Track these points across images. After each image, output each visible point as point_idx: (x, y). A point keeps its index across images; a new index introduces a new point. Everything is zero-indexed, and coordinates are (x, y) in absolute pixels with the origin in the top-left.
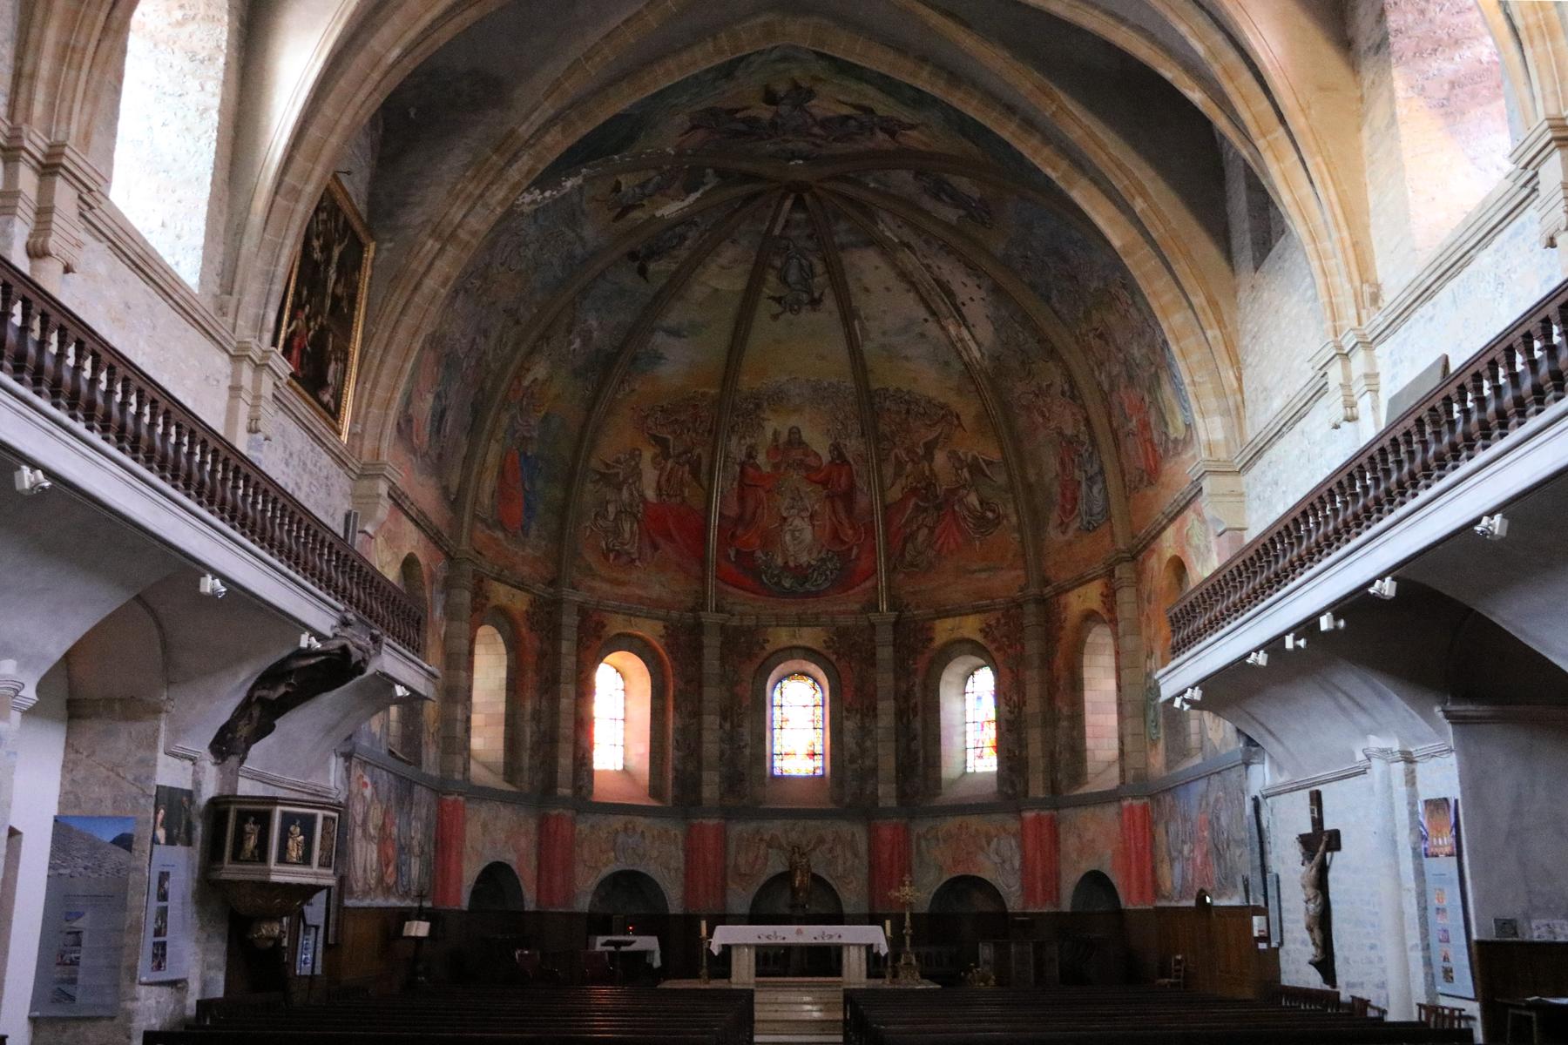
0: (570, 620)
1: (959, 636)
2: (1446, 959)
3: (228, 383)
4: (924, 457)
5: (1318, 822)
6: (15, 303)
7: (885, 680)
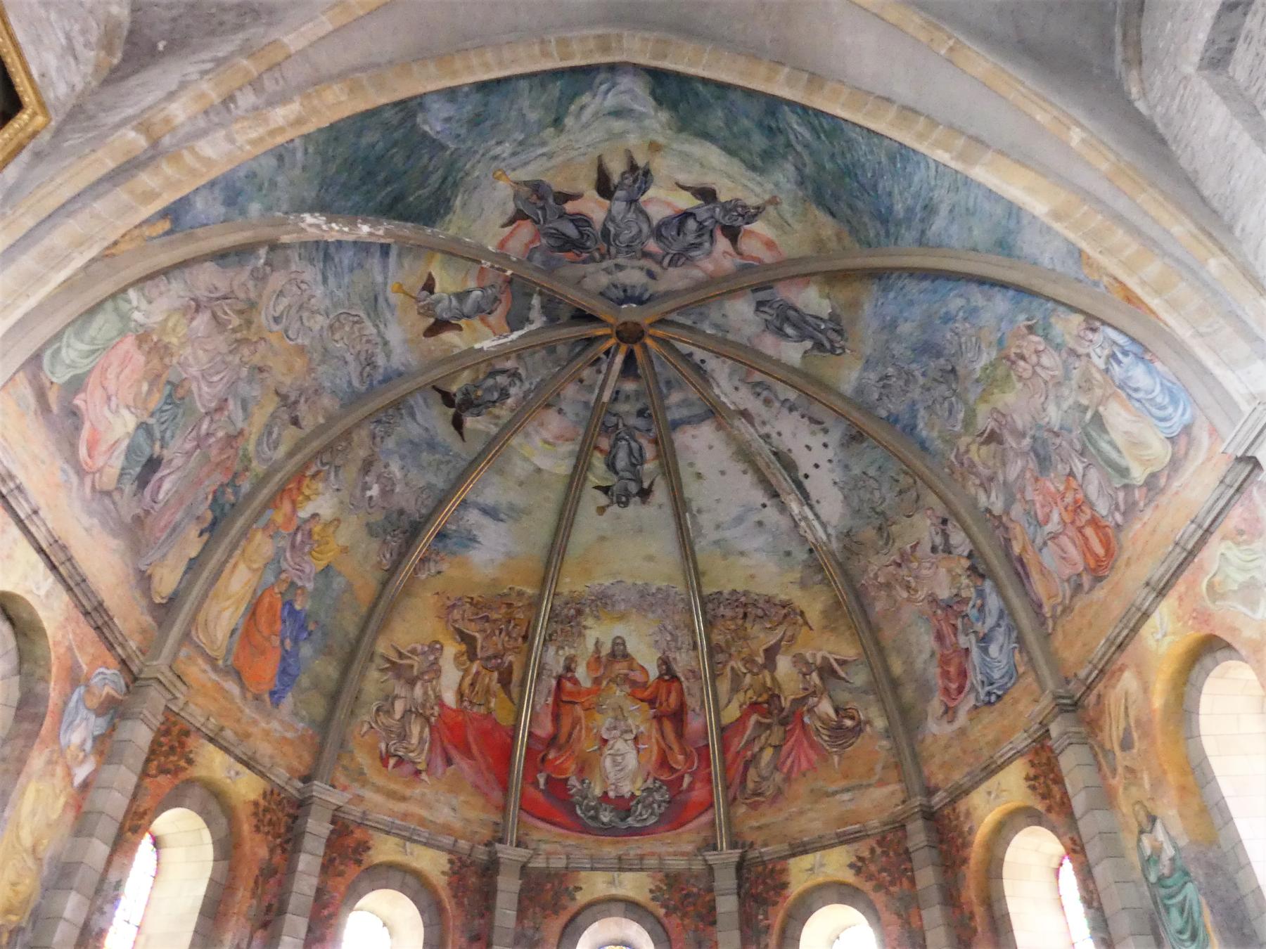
0: (317, 828)
1: (821, 879)
4: (764, 666)
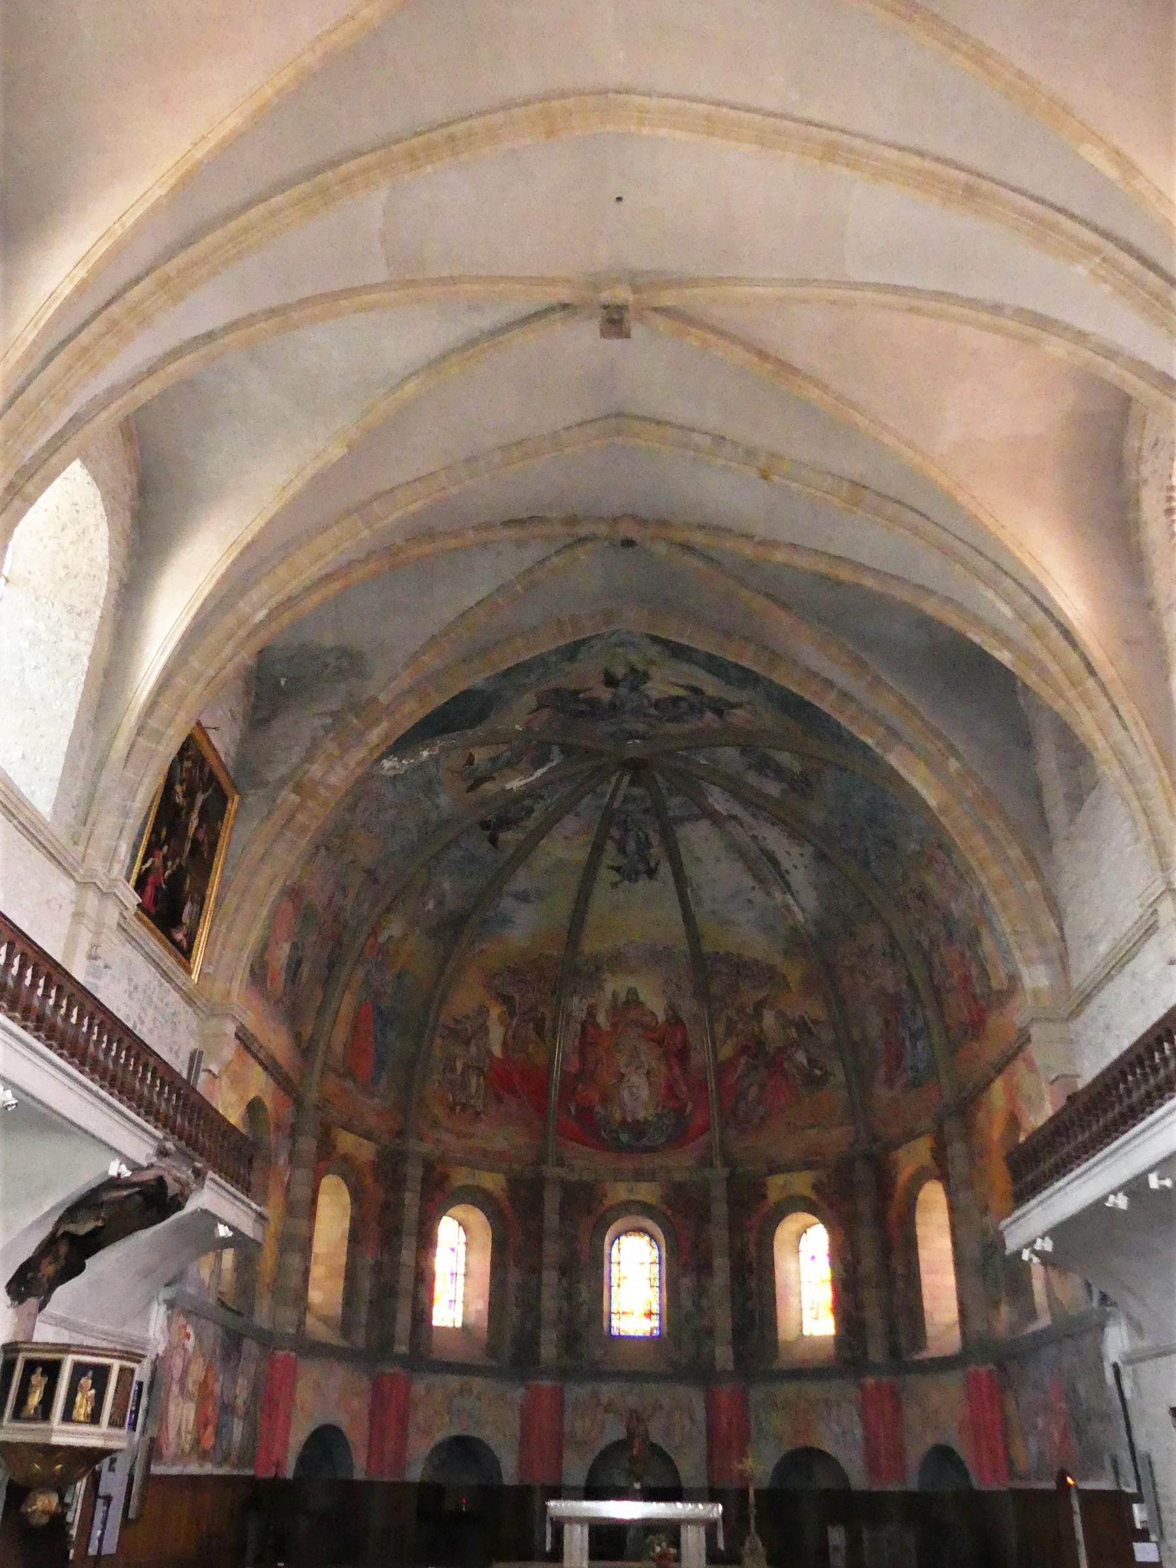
0: (415, 1172)
3: (71, 908)
7: (719, 1235)
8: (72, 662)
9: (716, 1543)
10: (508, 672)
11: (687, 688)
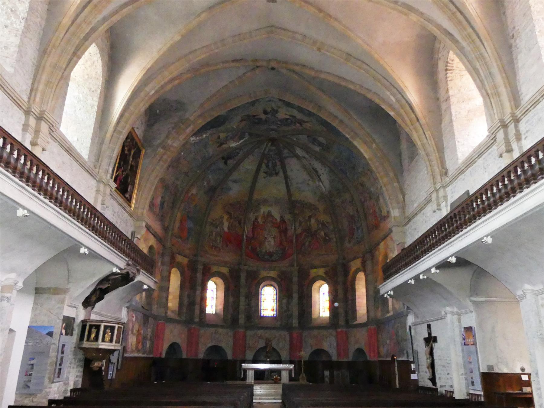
0: (200, 267)
2: (472, 378)
3: (95, 189)
5: (430, 334)
6: (40, 171)
8: (92, 108)
9: (292, 375)
10: (233, 110)
11: (290, 116)
